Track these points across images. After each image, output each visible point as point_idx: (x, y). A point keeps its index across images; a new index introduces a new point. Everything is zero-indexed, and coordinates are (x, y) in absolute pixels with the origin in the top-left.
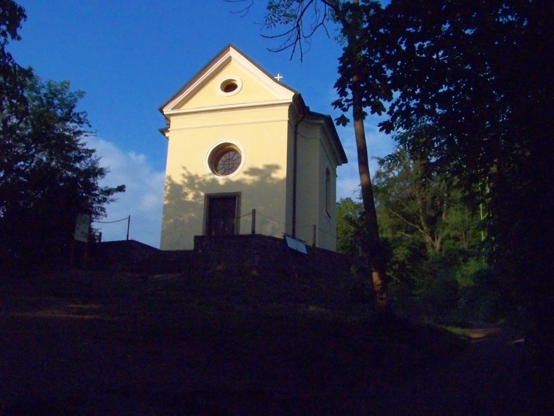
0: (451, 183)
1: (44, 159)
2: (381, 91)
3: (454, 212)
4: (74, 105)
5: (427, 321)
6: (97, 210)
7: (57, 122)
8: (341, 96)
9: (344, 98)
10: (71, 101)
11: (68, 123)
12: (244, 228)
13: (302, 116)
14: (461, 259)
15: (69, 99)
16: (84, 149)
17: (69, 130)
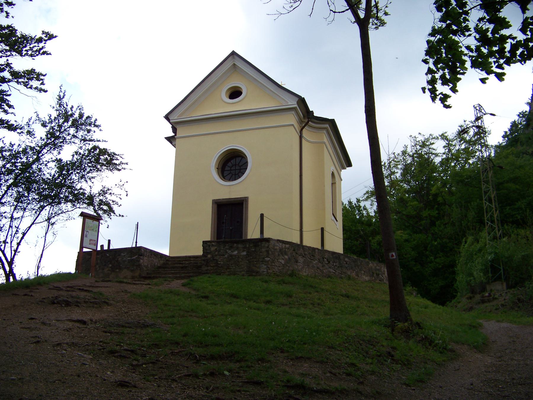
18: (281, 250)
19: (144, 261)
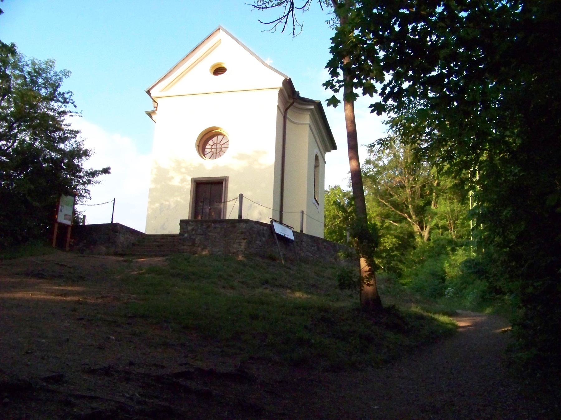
0: (442, 169)
1: (27, 139)
2: (373, 72)
3: (443, 201)
4: (59, 84)
5: (415, 309)
6: (81, 192)
7: (42, 102)
8: (332, 77)
9: (336, 79)
10: (56, 80)
11: (53, 103)
12: (231, 213)
13: (291, 101)
14: (449, 248)
15: (54, 78)
16: (68, 130)
17: (54, 110)
18: (258, 233)
19: (121, 238)
